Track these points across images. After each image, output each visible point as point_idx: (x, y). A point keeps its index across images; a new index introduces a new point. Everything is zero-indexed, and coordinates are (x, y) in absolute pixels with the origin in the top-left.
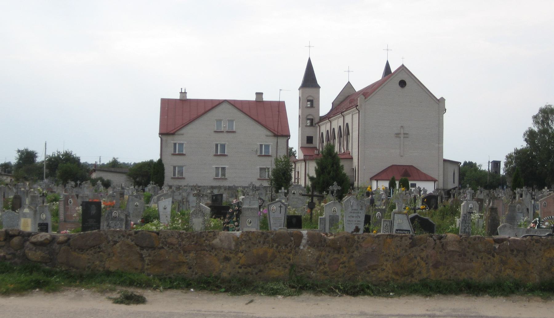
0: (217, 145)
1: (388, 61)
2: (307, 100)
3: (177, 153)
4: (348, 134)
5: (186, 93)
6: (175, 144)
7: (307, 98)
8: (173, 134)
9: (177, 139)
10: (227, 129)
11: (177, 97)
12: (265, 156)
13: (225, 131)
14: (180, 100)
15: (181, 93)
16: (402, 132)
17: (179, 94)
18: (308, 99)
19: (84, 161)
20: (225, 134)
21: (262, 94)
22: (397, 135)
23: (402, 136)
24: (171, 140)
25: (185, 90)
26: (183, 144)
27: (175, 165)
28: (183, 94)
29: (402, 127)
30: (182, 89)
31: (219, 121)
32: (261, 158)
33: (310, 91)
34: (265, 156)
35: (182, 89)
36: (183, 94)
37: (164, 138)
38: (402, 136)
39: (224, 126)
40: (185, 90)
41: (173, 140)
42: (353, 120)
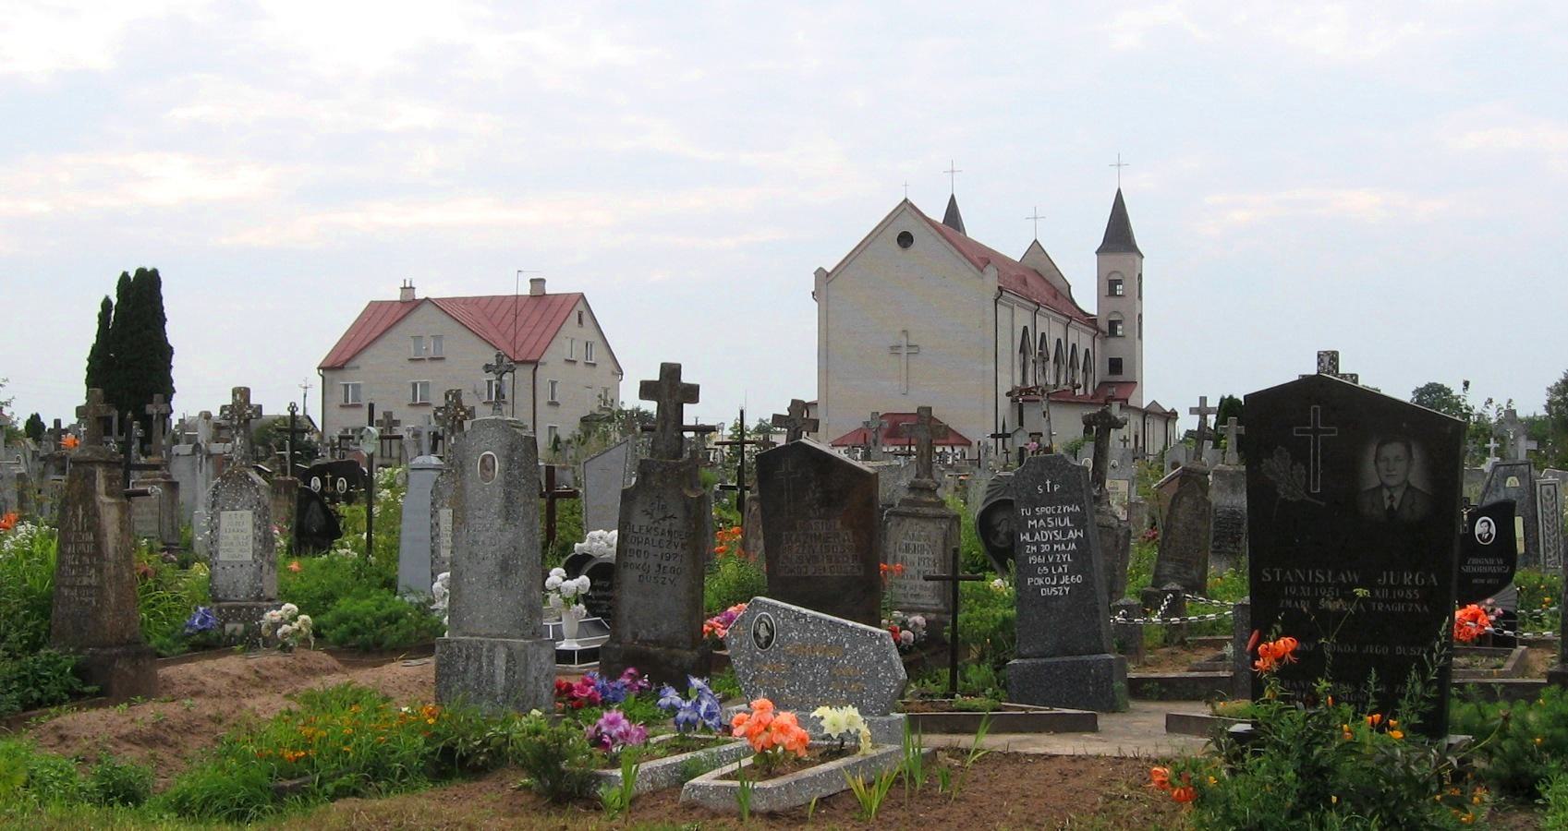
0: (415, 386)
1: (956, 197)
2: (1110, 281)
3: (350, 402)
4: (1023, 350)
5: (414, 288)
6: (347, 386)
7: (1107, 278)
8: (342, 368)
9: (351, 377)
10: (432, 354)
11: (396, 296)
12: (352, 406)
13: (426, 358)
14: (403, 302)
15: (404, 288)
16: (904, 343)
17: (399, 292)
18: (1111, 278)
19: (1544, 399)
20: (428, 365)
21: (543, 281)
22: (895, 349)
23: (904, 351)
24: (339, 380)
25: (411, 283)
26: (359, 386)
27: (346, 426)
28: (538, 282)
29: (904, 331)
30: (405, 281)
31: (418, 339)
32: (345, 411)
33: (1118, 261)
34: (352, 406)
35: (405, 281)
36: (538, 282)
37: (328, 376)
38: (904, 351)
39: (430, 348)
40: (411, 283)
41: (343, 380)
42: (388, 337)
